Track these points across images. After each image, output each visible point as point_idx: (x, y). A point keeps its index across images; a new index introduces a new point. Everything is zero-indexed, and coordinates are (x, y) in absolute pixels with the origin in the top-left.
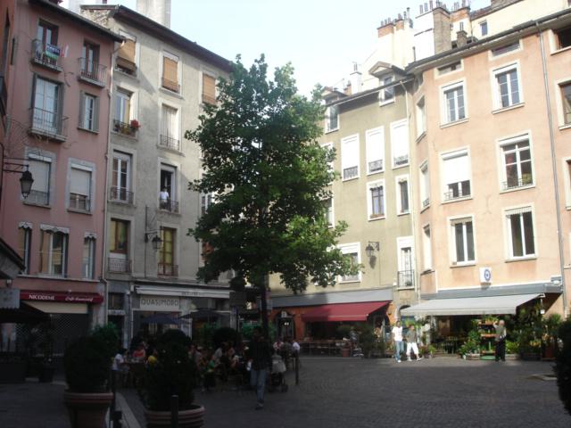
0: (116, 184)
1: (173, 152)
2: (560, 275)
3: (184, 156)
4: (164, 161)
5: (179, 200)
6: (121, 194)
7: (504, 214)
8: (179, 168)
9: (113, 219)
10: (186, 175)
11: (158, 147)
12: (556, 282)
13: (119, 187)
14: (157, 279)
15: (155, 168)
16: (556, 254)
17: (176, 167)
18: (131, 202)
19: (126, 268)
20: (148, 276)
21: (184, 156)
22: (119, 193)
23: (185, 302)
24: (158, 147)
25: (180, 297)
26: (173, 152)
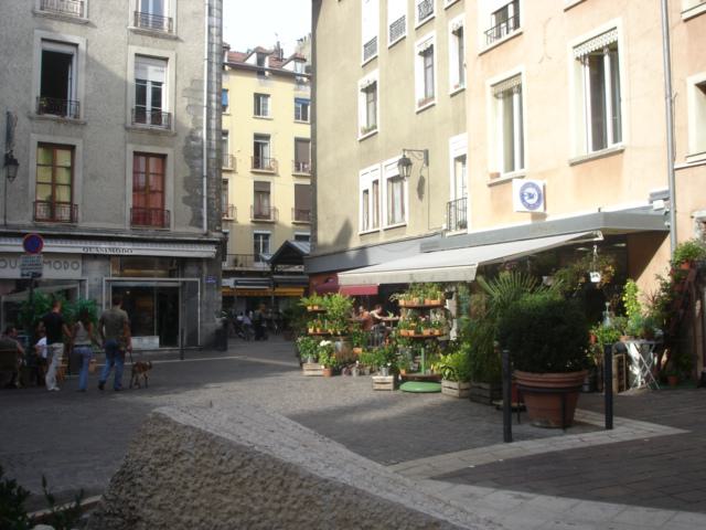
0: (144, 102)
1: (70, 20)
2: (666, 188)
3: (94, 26)
4: (47, 35)
5: (81, 98)
6: (153, 116)
7: (572, 55)
8: (82, 47)
9: (41, 144)
10: (97, 58)
11: (35, 14)
12: (659, 204)
13: (149, 106)
14: (30, 228)
15: (29, 47)
16: (660, 136)
17: (76, 45)
18: (169, 127)
19: (257, 216)
20: (8, 222)
21: (94, 26)
22: (148, 115)
23: (96, 265)
24: (35, 14)
25: (85, 257)
26: (70, 20)
